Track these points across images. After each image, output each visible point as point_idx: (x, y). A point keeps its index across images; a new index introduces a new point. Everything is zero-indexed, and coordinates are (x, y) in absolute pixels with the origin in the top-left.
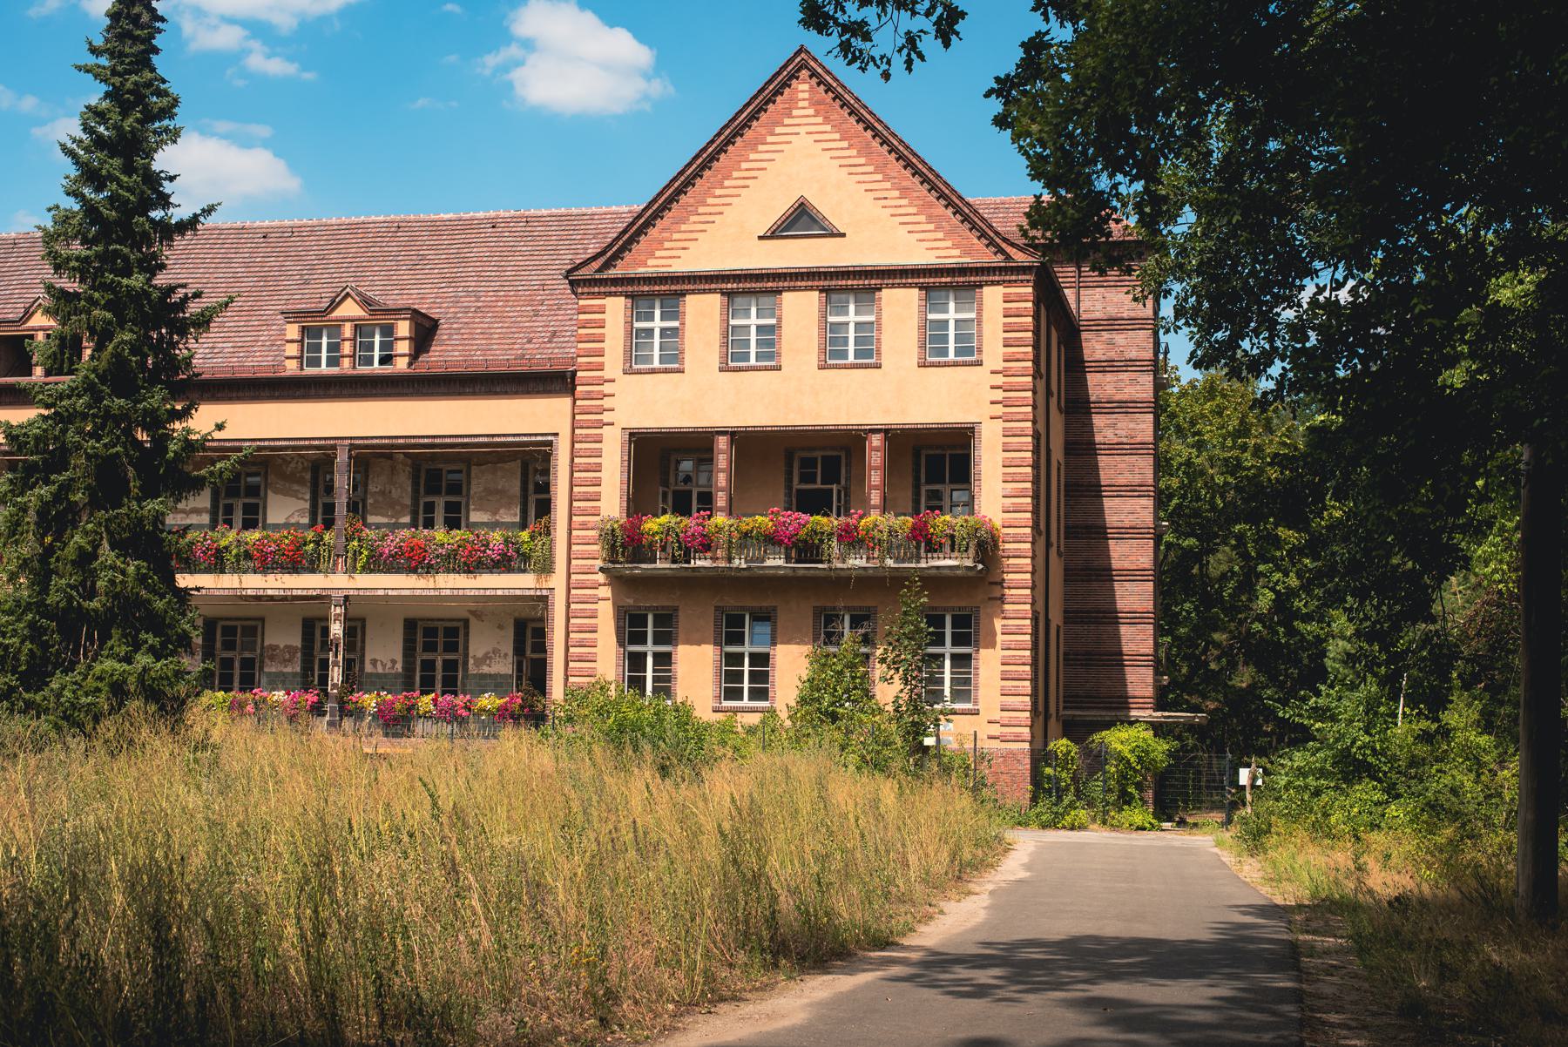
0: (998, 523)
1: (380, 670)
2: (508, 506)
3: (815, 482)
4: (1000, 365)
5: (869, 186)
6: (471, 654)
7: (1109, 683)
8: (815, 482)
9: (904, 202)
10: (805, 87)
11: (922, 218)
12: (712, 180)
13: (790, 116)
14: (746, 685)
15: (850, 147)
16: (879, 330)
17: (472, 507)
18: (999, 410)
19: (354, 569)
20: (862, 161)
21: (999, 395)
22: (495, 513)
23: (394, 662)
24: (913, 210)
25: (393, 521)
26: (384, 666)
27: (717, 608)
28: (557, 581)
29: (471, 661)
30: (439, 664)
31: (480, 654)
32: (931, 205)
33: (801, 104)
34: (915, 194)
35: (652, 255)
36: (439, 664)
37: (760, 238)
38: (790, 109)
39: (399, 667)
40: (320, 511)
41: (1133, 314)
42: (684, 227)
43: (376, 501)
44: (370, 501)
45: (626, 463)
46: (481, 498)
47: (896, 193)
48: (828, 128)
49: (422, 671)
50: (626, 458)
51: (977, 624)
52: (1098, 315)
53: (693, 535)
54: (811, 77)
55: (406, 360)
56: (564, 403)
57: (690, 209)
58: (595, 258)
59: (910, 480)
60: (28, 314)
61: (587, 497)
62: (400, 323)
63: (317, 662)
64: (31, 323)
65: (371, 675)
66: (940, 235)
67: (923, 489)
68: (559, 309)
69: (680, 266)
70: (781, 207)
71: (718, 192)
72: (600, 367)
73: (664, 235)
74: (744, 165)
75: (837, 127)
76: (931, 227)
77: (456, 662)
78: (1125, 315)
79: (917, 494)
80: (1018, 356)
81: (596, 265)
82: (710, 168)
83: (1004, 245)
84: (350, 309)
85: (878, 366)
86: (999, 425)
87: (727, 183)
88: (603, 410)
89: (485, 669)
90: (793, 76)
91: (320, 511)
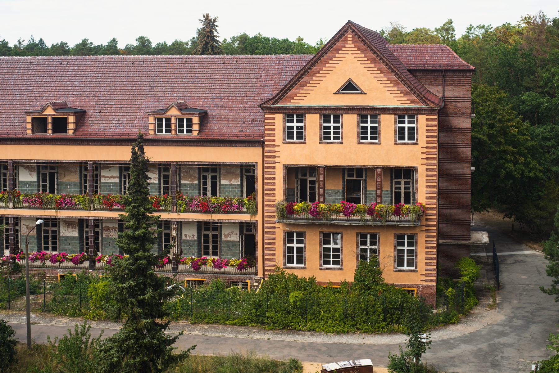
0: (424, 204)
1: (188, 238)
2: (236, 179)
3: (353, 177)
4: (425, 145)
5: (375, 75)
6: (223, 233)
7: (454, 230)
8: (353, 177)
9: (389, 82)
10: (350, 36)
11: (395, 88)
12: (315, 70)
13: (345, 47)
14: (331, 259)
15: (368, 60)
16: (380, 130)
17: (221, 178)
18: (425, 161)
19: (180, 211)
20: (372, 65)
21: (425, 156)
22: (230, 181)
23: (193, 236)
24: (392, 85)
25: (191, 183)
26: (190, 237)
27: (320, 232)
28: (259, 218)
29: (223, 236)
30: (211, 236)
31: (226, 233)
32: (399, 84)
33: (349, 42)
34: (393, 79)
35: (293, 99)
36: (211, 236)
37: (334, 93)
38: (345, 44)
39: (196, 237)
40: (162, 178)
41: (464, 96)
42: (305, 88)
43: (184, 175)
44: (182, 175)
45: (285, 177)
46: (225, 175)
47: (386, 79)
48: (359, 52)
49: (204, 238)
50: (285, 175)
51: (417, 239)
52: (450, 96)
53: (313, 211)
54: (352, 32)
55: (197, 132)
56: (259, 150)
57: (307, 81)
58: (272, 99)
59: (389, 178)
60: (44, 109)
61: (269, 190)
62: (194, 118)
63: (163, 234)
64: (45, 113)
65: (185, 240)
66: (402, 95)
67: (394, 181)
68: (254, 107)
69: (305, 103)
70: (342, 82)
71: (318, 75)
72: (274, 141)
73: (297, 91)
74: (327, 65)
75: (362, 52)
76: (399, 92)
77: (217, 235)
78: (461, 96)
79: (391, 183)
80: (431, 142)
81: (271, 102)
82: (314, 66)
83: (426, 101)
84: (174, 112)
85: (379, 144)
86: (425, 167)
87: (321, 72)
88: (275, 151)
89: (229, 239)
90: (346, 31)
91: (162, 178)
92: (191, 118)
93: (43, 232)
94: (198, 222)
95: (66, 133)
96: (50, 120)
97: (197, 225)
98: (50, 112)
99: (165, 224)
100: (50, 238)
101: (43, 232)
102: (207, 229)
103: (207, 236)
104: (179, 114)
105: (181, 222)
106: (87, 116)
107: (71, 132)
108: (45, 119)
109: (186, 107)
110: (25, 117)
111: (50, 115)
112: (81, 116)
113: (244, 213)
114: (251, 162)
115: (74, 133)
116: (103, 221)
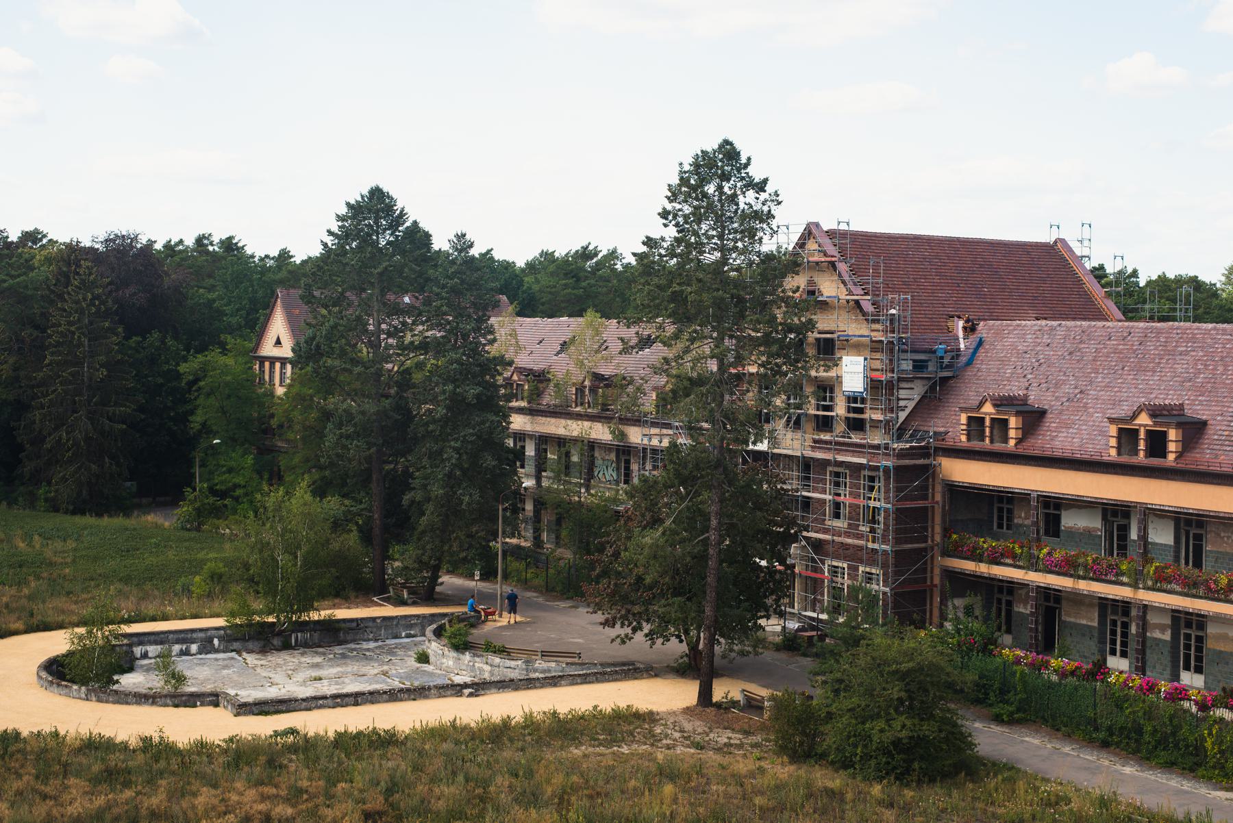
40: (1191, 539)
62: (1170, 430)
64: (1137, 422)
91: (1191, 539)
92: (1007, 419)
93: (1182, 638)
94: (1173, 611)
95: (1165, 457)
96: (1142, 435)
97: (1172, 616)
98: (1144, 420)
99: (1123, 606)
100: (1193, 649)
101: (1182, 638)
102: (1189, 625)
103: (1188, 637)
104: (993, 411)
105: (1145, 606)
106: (1209, 432)
107: (1171, 457)
108: (1136, 432)
109: (1182, 412)
110: (1108, 427)
111: (1142, 425)
112: (1034, 418)
113: (1122, 584)
114: (1187, 508)
115: (1176, 459)
116: (1209, 618)
